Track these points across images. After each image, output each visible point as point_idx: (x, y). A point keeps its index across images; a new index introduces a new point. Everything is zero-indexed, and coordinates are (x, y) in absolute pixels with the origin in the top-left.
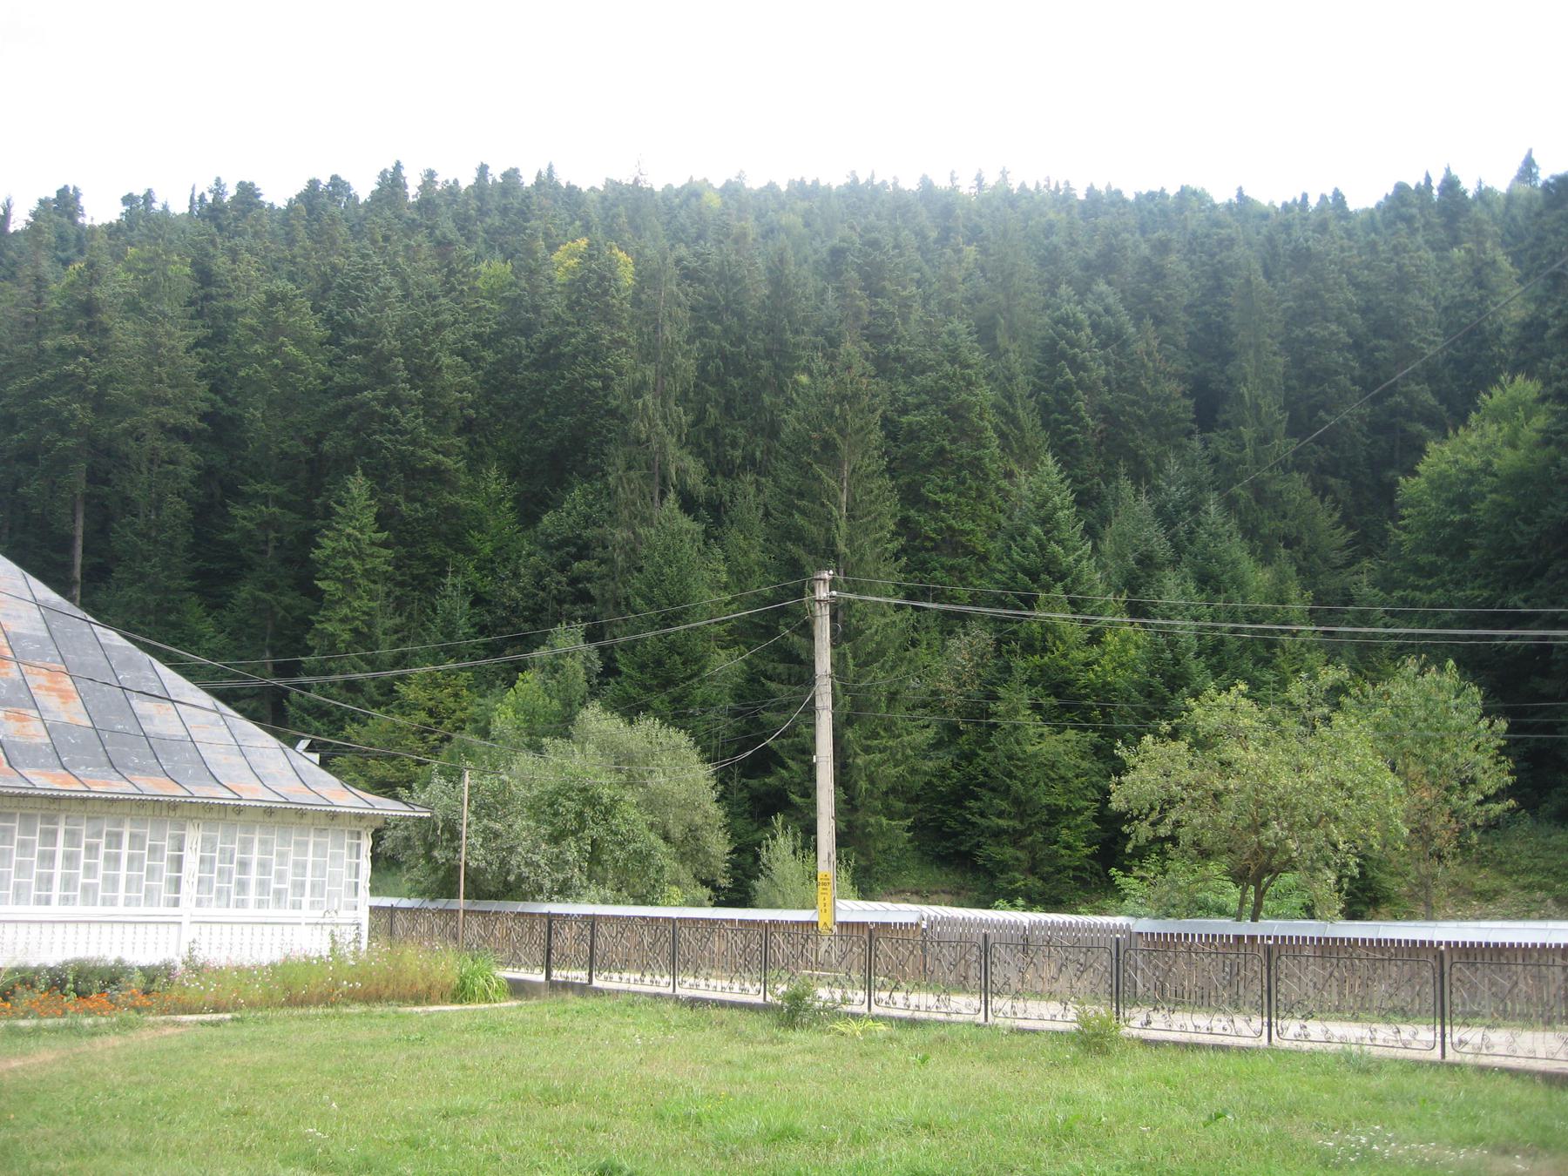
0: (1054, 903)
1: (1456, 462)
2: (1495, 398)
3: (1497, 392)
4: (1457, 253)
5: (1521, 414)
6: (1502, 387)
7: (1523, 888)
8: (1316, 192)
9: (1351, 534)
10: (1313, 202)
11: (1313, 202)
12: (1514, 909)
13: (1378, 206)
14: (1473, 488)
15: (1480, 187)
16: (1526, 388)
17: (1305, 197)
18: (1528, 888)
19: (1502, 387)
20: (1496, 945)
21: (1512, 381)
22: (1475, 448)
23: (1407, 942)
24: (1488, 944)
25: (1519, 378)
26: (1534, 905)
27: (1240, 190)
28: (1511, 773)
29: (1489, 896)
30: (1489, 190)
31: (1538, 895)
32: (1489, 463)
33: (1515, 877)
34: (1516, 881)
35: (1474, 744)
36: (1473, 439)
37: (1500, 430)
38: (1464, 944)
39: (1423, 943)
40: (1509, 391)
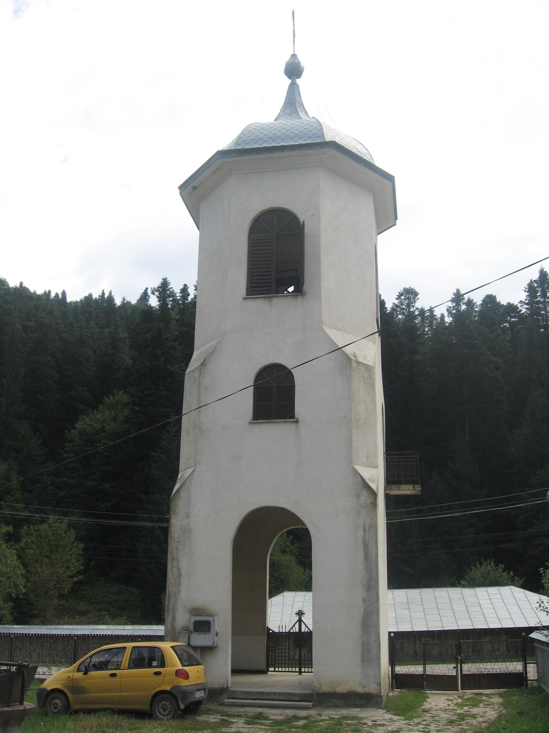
0: (292, 529)
1: (91, 425)
2: (109, 400)
3: (111, 397)
4: (106, 331)
5: (120, 408)
6: (114, 395)
7: (98, 610)
8: (55, 290)
9: (46, 450)
10: (53, 295)
11: (53, 295)
12: (93, 619)
13: (81, 300)
14: (96, 437)
15: (123, 301)
16: (122, 396)
17: (50, 292)
18: (100, 610)
19: (114, 395)
20: (53, 635)
21: (118, 394)
22: (99, 420)
23: (20, 634)
24: (50, 635)
25: (121, 392)
26: (101, 617)
27: (21, 283)
28: (82, 565)
29: (83, 613)
30: (129, 303)
31: (103, 613)
32: (104, 427)
33: (95, 605)
34: (95, 607)
35: (70, 553)
36: (99, 416)
37: (110, 413)
38: (41, 634)
39: (26, 634)
40: (116, 397)
